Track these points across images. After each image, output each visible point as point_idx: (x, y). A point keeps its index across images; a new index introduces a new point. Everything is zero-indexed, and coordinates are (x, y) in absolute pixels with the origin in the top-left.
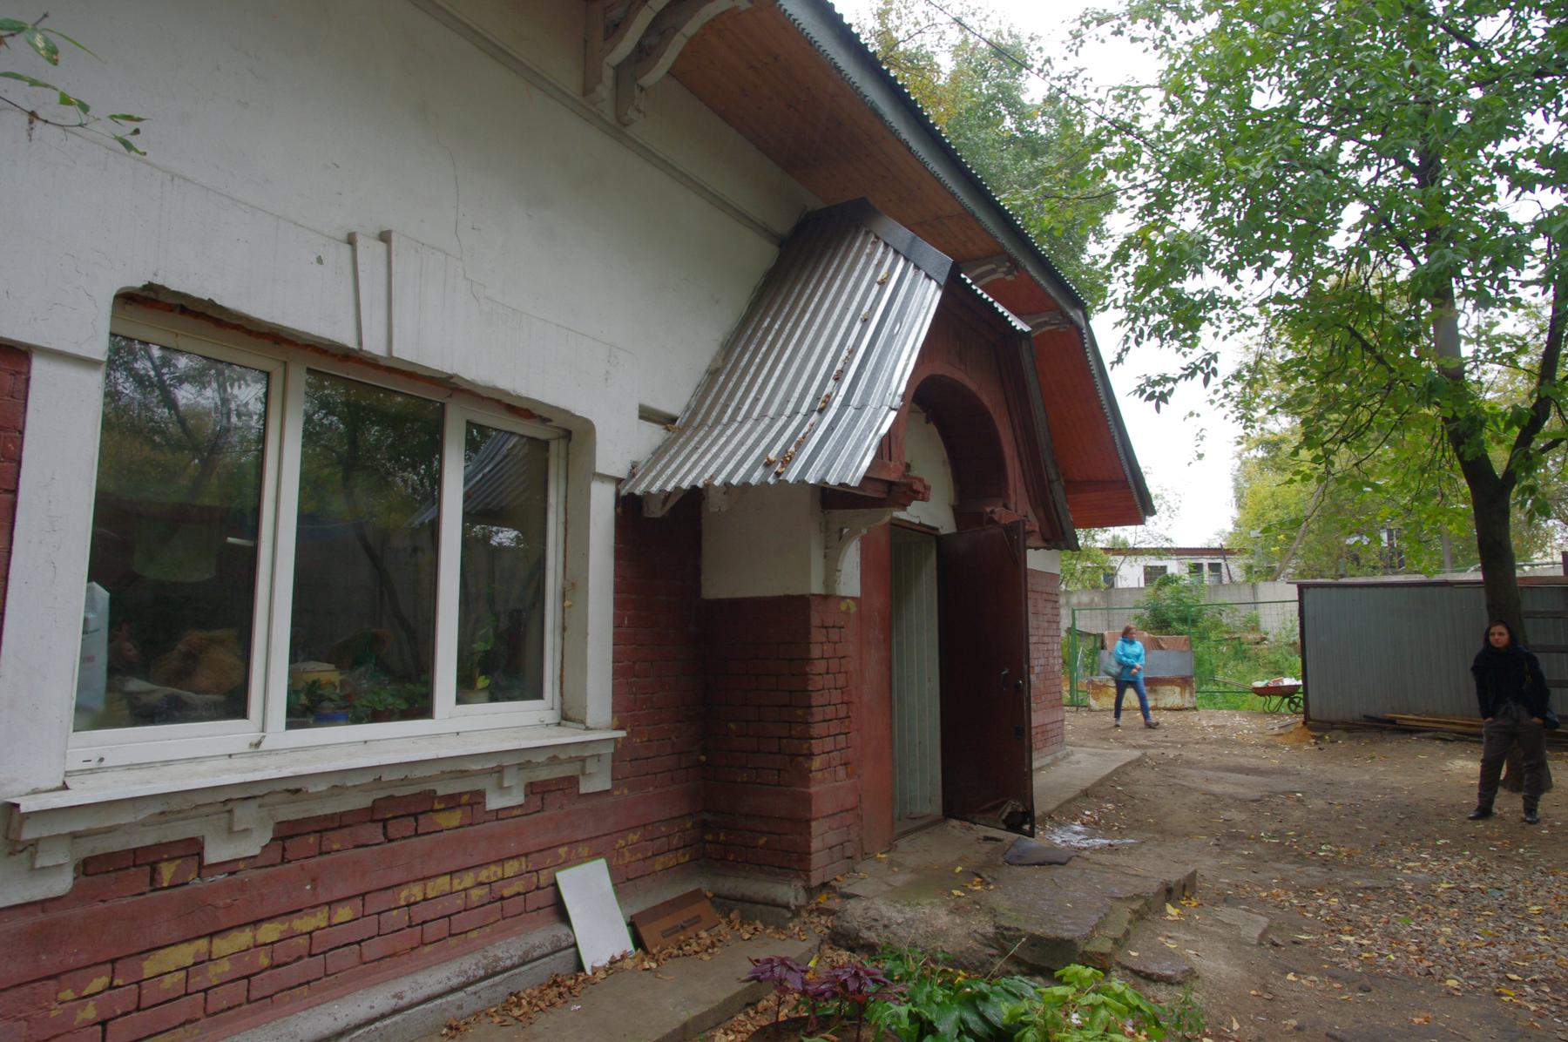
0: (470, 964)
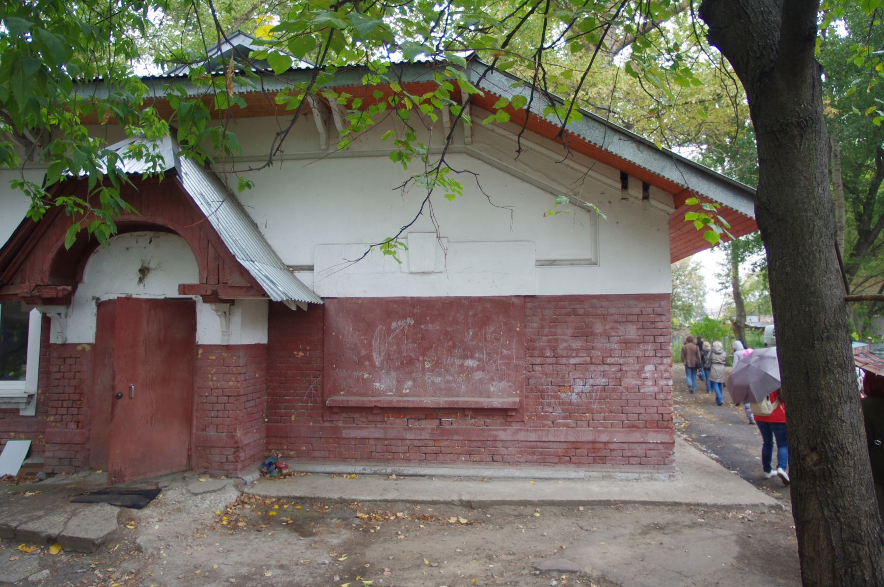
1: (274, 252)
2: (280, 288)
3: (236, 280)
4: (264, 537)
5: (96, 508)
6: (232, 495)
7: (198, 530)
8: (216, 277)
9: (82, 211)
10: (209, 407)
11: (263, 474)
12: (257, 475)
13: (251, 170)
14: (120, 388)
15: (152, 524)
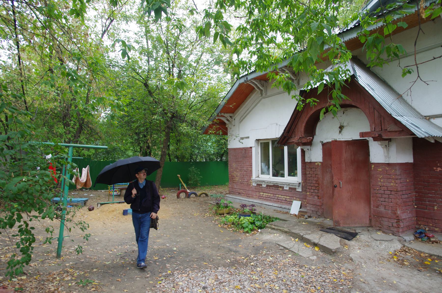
0: (280, 206)
1: (414, 109)
2: (422, 130)
3: (392, 127)
4: (424, 275)
5: (330, 235)
6: (398, 246)
7: (380, 259)
8: (380, 127)
9: (316, 104)
10: (380, 195)
11: (416, 238)
12: (412, 238)
13: (435, 59)
14: (336, 183)
15: (356, 249)
